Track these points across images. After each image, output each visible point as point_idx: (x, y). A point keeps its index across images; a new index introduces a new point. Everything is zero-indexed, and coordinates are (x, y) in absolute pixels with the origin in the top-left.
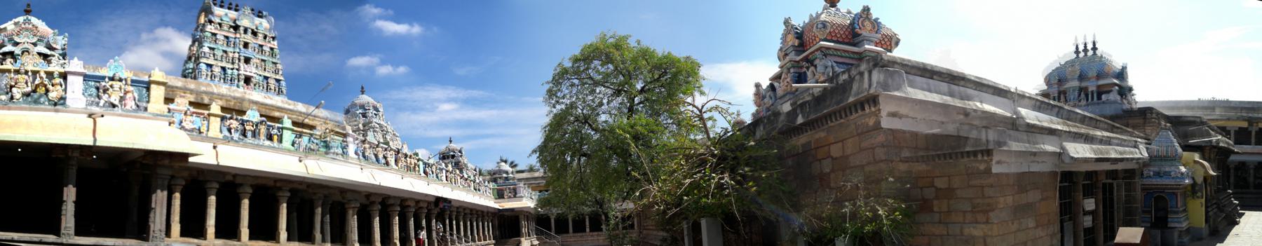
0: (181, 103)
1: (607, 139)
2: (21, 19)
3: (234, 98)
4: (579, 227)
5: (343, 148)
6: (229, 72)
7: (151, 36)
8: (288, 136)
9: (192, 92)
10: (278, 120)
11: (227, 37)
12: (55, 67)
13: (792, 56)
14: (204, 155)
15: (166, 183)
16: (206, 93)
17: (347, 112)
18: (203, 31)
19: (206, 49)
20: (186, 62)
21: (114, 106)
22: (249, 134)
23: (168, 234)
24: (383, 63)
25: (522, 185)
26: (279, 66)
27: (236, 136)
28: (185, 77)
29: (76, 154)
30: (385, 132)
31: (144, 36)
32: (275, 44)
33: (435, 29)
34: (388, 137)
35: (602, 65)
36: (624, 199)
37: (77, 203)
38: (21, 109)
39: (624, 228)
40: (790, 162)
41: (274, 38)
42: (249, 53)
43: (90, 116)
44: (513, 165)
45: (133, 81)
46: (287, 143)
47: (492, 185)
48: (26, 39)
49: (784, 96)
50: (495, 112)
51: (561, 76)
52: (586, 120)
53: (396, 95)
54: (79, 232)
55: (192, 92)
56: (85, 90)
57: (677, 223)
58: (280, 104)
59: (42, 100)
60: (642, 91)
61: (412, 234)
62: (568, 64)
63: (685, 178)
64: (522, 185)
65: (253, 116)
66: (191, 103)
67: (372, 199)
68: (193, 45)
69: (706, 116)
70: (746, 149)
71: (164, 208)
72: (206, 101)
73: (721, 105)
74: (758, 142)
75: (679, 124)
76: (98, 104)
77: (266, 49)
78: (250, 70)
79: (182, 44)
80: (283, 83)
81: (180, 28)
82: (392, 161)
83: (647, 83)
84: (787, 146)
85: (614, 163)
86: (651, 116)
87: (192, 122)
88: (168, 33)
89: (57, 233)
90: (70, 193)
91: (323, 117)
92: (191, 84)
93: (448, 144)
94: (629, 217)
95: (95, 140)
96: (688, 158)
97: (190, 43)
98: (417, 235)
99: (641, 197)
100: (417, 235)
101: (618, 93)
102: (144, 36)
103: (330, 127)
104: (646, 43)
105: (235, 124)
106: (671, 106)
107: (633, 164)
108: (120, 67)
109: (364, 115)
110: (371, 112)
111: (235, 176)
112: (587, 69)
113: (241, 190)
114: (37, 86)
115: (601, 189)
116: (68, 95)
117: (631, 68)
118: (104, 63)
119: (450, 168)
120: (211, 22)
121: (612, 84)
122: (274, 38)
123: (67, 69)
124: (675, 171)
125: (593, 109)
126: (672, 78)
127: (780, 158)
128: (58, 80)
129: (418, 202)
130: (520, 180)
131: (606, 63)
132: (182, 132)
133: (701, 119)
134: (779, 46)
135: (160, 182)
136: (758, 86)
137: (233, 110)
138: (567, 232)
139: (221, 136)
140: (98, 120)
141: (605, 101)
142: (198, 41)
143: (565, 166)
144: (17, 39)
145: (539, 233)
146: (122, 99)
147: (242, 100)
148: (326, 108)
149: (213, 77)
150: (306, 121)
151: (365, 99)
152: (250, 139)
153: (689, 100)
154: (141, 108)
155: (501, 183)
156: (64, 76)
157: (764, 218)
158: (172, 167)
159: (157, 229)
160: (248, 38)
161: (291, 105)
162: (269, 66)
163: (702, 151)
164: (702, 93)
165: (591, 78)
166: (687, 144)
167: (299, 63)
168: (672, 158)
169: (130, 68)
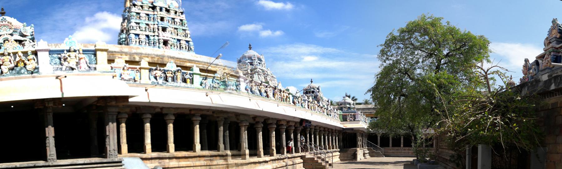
0: (120, 62)
1: (420, 86)
4: (396, 143)
5: (237, 86)
6: (152, 38)
7: (93, 19)
8: (197, 79)
9: (126, 54)
11: (148, 15)
12: (29, 47)
13: (554, 44)
14: (139, 96)
15: (115, 117)
16: (136, 54)
17: (240, 61)
19: (133, 24)
20: (120, 34)
21: (73, 69)
23: (120, 151)
24: (265, 28)
25: (359, 113)
26: (188, 32)
27: (161, 81)
28: (120, 44)
29: (51, 105)
30: (266, 75)
31: (88, 19)
32: (183, 17)
33: (303, 6)
34: (268, 79)
35: (421, 36)
36: (428, 127)
38: (9, 79)
39: (426, 146)
40: (542, 114)
42: (165, 24)
43: (57, 78)
44: (354, 99)
45: (84, 51)
47: (339, 112)
48: (5, 32)
49: (544, 70)
50: (343, 63)
51: (391, 41)
52: (406, 72)
53: (274, 50)
54: (59, 157)
55: (126, 54)
57: (463, 146)
59: (23, 71)
60: (447, 55)
61: (284, 144)
62: (397, 34)
63: (471, 116)
64: (359, 113)
66: (127, 62)
67: (257, 120)
69: (489, 76)
70: (514, 101)
71: (115, 134)
72: (137, 59)
73: (501, 70)
74: (523, 98)
75: (470, 80)
76: (61, 69)
77: (177, 20)
78: (166, 36)
80: (191, 43)
81: (112, 11)
82: (271, 94)
83: (451, 51)
84: (542, 103)
85: (423, 102)
86: (451, 73)
87: (130, 74)
88: (105, 15)
89: (45, 158)
90: (50, 132)
91: (222, 65)
92: (125, 48)
93: (310, 83)
94: (431, 139)
95: (63, 94)
96: (474, 103)
97: (121, 20)
98: (287, 144)
99: (440, 126)
100: (287, 144)
101: (430, 55)
102: (88, 19)
103: (226, 71)
104: (452, 24)
105: (159, 73)
106: (466, 67)
107: (436, 104)
109: (251, 64)
110: (256, 62)
111: (162, 108)
112: (410, 38)
113: (167, 118)
114: (18, 62)
115: (413, 119)
116: (40, 66)
117: (441, 40)
118: (62, 40)
119: (311, 99)
120: (134, 5)
121: (427, 49)
122: (182, 13)
123: (37, 48)
124: (464, 111)
125: (412, 65)
126: (469, 49)
127: (536, 110)
128: (31, 57)
129: (288, 122)
130: (358, 109)
131: (423, 35)
132: (123, 81)
133: (486, 78)
134: (546, 36)
135: (110, 117)
136: (526, 61)
137: (157, 64)
138: (388, 146)
140: (63, 80)
141: (420, 60)
143: (390, 102)
145: (369, 145)
146: (78, 64)
147: (163, 57)
148: (223, 58)
149: (140, 42)
150: (210, 68)
151: (251, 53)
153: (479, 65)
155: (345, 110)
156: (35, 53)
157: (521, 148)
158: (117, 106)
160: (164, 14)
162: (181, 32)
163: (484, 99)
164: (488, 61)
165: (412, 44)
166: (474, 93)
167: (202, 29)
168: (463, 102)
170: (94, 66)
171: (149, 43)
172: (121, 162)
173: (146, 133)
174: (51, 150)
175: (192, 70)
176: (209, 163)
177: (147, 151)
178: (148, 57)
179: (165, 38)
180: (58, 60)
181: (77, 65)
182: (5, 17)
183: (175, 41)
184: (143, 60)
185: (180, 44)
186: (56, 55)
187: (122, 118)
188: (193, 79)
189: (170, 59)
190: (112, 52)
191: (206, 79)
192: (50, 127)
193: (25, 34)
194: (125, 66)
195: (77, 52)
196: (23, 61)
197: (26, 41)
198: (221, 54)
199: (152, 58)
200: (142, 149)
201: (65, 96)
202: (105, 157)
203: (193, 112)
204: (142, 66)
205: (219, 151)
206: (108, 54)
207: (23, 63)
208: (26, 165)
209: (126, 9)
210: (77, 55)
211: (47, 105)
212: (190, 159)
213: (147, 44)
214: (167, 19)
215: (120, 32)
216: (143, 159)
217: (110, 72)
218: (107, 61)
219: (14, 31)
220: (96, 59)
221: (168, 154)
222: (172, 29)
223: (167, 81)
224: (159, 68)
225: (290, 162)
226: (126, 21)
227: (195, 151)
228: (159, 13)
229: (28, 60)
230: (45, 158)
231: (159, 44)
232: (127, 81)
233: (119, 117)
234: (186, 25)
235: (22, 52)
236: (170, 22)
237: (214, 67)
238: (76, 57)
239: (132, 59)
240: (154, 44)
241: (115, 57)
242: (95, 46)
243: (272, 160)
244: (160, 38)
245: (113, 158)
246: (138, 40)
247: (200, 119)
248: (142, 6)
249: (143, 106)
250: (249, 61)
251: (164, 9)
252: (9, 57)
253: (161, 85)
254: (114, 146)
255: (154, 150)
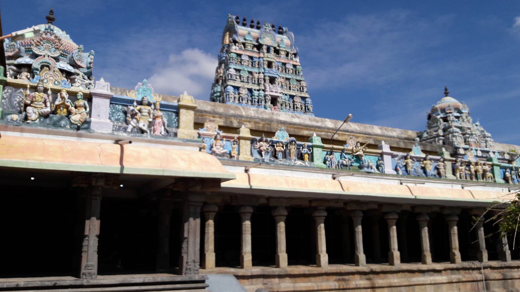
0: (211, 128)
2: (42, 27)
3: (263, 120)
6: (256, 93)
8: (319, 154)
9: (220, 115)
10: (307, 138)
11: (251, 58)
12: (79, 88)
14: (237, 179)
15: (199, 210)
16: (235, 116)
18: (228, 52)
19: (232, 71)
20: (214, 85)
21: (143, 132)
22: (280, 155)
23: (202, 264)
26: (304, 84)
27: (267, 158)
28: (213, 100)
29: (101, 183)
31: (172, 58)
37: (101, 237)
41: (295, 55)
42: (273, 72)
43: (117, 142)
45: (162, 106)
46: (318, 161)
48: (46, 52)
54: (102, 270)
56: (112, 115)
58: (308, 122)
59: (63, 123)
65: (282, 136)
66: (221, 128)
68: (219, 68)
71: (198, 236)
72: (235, 124)
76: (125, 130)
77: (289, 67)
78: (275, 90)
79: (210, 67)
80: (309, 100)
81: (206, 50)
89: (76, 272)
90: (93, 227)
92: (220, 108)
95: (122, 168)
97: (216, 65)
102: (172, 58)
103: (360, 140)
105: (265, 146)
108: (147, 90)
109: (445, 120)
111: (269, 199)
114: (58, 107)
116: (93, 119)
118: (131, 86)
120: (235, 42)
122: (295, 55)
123: (93, 91)
128: (81, 102)
137: (263, 132)
139: (252, 159)
140: (126, 147)
142: (224, 63)
144: (36, 51)
146: (151, 124)
147: (270, 121)
148: (354, 121)
149: (240, 99)
150: (336, 137)
152: (281, 160)
154: (171, 134)
156: (89, 97)
159: (190, 260)
160: (271, 56)
161: (319, 122)
169: (159, 92)
170: (174, 130)
171: (252, 101)
172: (203, 282)
173: (244, 236)
174: (90, 257)
175: (311, 141)
176: (343, 285)
177: (245, 264)
178: (250, 122)
179: (274, 94)
180: (122, 114)
181: (149, 127)
182: (52, 27)
183: (287, 98)
184: (243, 127)
185: (294, 102)
186: (120, 107)
187: (209, 212)
188: (312, 153)
189: (280, 125)
190: (201, 111)
191: (331, 154)
192: (94, 219)
193: (79, 63)
194: (218, 134)
195: (153, 106)
196: (67, 107)
197: (78, 75)
198: (350, 115)
199: (256, 123)
200: (238, 262)
201: (125, 172)
202: (179, 272)
203: (314, 204)
204: (242, 135)
205: (357, 264)
206: (195, 115)
207: (65, 110)
208: (39, 284)
209: (224, 48)
210: (152, 111)
211: (94, 183)
212: (312, 279)
213: (250, 103)
214: (277, 64)
215: (214, 82)
216: (238, 277)
217: (197, 141)
218: (192, 125)
219: (61, 55)
220: (178, 121)
221: (277, 269)
222: (282, 80)
223: (276, 158)
224: (264, 139)
225: (495, 275)
226: (223, 65)
227: (319, 266)
228: (266, 54)
229: (76, 107)
230: (76, 272)
231: (266, 102)
232: (220, 156)
233: (205, 210)
234: (301, 74)
235: (68, 92)
236: (281, 69)
237: (343, 135)
238: (149, 113)
239: (228, 125)
240: (258, 102)
241: (205, 119)
242: (179, 101)
243: (452, 269)
244: (267, 93)
245: (192, 275)
246: (237, 96)
247: (325, 214)
248: (244, 44)
249: (241, 195)
250: (442, 115)
251: (272, 49)
252: (45, 96)
253: (267, 163)
254: (195, 254)
255: (256, 262)
